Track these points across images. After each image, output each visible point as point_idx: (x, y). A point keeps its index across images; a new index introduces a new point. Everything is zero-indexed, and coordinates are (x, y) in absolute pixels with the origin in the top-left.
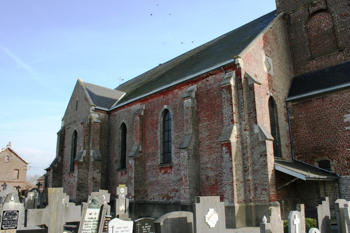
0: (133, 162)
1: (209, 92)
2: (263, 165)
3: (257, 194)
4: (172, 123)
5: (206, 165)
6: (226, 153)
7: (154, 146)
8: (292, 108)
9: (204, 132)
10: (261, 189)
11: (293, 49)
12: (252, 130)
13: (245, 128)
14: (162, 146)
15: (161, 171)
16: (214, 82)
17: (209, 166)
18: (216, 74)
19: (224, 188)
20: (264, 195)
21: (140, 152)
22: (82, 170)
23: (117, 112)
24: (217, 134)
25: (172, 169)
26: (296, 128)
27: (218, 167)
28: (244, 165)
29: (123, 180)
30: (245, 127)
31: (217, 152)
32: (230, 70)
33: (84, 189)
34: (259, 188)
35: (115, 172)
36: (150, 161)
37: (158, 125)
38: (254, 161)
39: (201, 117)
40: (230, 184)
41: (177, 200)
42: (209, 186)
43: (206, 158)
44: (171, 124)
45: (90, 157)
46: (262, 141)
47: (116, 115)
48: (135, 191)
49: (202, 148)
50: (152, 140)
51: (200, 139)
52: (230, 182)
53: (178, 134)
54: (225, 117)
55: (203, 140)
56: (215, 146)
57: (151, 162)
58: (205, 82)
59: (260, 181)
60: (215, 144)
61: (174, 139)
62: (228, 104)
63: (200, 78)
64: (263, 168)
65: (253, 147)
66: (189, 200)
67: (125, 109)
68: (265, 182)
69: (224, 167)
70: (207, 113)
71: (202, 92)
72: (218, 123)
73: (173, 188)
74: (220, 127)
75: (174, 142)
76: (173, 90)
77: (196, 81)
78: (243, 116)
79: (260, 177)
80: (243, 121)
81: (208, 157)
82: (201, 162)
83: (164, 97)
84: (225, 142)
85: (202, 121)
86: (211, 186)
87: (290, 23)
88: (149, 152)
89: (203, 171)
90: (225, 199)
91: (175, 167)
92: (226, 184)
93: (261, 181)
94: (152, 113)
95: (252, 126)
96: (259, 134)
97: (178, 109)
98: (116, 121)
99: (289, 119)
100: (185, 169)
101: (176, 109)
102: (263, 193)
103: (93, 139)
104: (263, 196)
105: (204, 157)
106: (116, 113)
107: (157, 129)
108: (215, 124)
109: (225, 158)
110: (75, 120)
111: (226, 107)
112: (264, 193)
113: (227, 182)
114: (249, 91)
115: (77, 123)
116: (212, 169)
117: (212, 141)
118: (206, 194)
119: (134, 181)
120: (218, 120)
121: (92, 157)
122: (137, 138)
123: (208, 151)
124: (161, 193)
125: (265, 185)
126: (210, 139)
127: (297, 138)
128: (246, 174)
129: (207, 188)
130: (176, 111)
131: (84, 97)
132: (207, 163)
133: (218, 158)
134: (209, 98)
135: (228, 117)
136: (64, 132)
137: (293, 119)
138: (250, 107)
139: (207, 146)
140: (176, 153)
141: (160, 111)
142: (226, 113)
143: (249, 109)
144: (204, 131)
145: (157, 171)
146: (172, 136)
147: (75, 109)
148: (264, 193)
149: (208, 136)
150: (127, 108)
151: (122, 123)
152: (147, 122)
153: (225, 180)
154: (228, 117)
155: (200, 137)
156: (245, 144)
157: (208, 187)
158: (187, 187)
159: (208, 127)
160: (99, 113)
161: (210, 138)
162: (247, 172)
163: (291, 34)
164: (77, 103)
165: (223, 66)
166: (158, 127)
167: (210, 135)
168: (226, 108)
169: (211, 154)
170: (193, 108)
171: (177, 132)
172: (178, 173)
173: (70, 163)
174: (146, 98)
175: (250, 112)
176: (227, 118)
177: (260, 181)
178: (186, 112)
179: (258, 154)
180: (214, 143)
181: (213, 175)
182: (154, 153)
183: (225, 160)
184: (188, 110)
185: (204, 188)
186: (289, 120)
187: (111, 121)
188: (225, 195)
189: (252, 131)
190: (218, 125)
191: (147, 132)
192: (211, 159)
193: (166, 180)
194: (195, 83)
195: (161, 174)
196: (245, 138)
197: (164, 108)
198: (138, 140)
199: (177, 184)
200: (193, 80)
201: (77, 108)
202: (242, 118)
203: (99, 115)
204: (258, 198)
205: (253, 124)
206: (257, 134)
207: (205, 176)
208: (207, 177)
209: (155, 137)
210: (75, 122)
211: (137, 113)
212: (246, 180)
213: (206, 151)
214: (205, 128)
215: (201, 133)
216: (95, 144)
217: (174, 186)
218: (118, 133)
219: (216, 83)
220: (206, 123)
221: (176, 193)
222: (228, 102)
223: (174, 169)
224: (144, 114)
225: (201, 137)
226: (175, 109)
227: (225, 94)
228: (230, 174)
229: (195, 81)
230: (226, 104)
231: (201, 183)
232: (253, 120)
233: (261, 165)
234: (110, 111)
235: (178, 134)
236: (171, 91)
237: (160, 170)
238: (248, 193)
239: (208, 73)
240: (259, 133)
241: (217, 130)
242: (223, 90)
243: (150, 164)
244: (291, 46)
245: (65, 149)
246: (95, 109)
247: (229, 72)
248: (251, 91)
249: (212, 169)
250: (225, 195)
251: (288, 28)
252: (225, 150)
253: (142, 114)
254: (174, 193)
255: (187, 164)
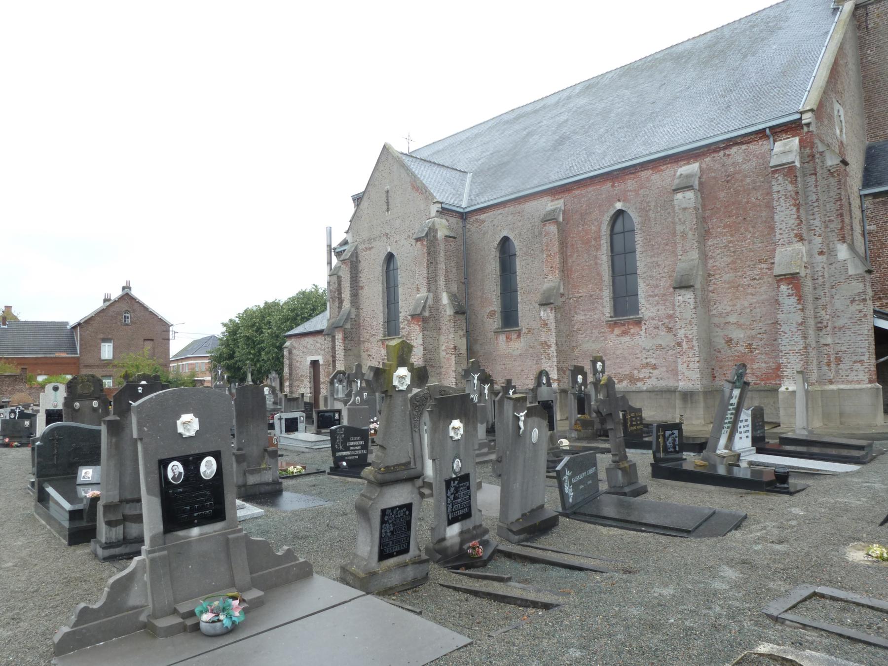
0: (550, 314)
1: (731, 179)
2: (856, 317)
3: (840, 371)
4: (639, 238)
5: (724, 317)
6: (788, 296)
7: (593, 283)
8: (872, 209)
9: (719, 256)
10: (851, 361)
11: (871, 83)
12: (832, 253)
13: (820, 250)
14: (611, 284)
15: (613, 330)
16: (744, 159)
17: (732, 319)
18: (751, 142)
19: (783, 359)
20: (857, 371)
21: (562, 295)
22: (428, 333)
23: (485, 215)
24: (752, 261)
25: (641, 327)
26: (878, 249)
27: (753, 321)
28: (816, 317)
29: (514, 350)
30: (820, 248)
31: (753, 295)
32: (784, 136)
33: (434, 370)
34: (846, 359)
35: (491, 335)
36: (582, 313)
37: (600, 241)
38: (835, 311)
39: (713, 228)
40: (797, 353)
41: (654, 384)
42: (732, 356)
43: (725, 305)
44: (636, 240)
45: (441, 307)
46: (855, 275)
47: (483, 221)
48: (558, 370)
49: (715, 286)
50: (588, 272)
51: (710, 270)
52: (799, 349)
53: (655, 259)
54: (780, 229)
55: (719, 272)
56: (746, 283)
57: (585, 314)
58: (721, 158)
59: (848, 347)
60: (748, 279)
61: (644, 270)
62: (788, 204)
63: (708, 150)
64: (857, 322)
65: (833, 284)
66: (699, 383)
67: (507, 209)
68: (859, 349)
69: (782, 322)
70: (727, 220)
71: (715, 178)
72: (755, 240)
73: (644, 361)
74: (759, 247)
75: (645, 275)
76: (639, 171)
77: (700, 155)
78: (816, 226)
79: (850, 340)
80: (816, 237)
81: (730, 303)
82: (714, 312)
83: (613, 186)
84: (787, 277)
85: (714, 235)
86: (738, 357)
87: (867, 27)
88: (580, 295)
89: (718, 330)
90: (785, 379)
91: (647, 323)
92: (789, 352)
93: (851, 347)
94: (585, 217)
95: (831, 246)
96: (849, 260)
97: (651, 212)
98: (484, 234)
99: (866, 231)
100: (689, 326)
101: (647, 211)
102: (855, 368)
103: (447, 271)
104: (855, 373)
105: (720, 303)
106: (483, 217)
107: (597, 249)
108: (747, 242)
109: (785, 305)
110: (388, 232)
111: (783, 209)
112: (857, 367)
113: (789, 348)
114: (826, 178)
115: (392, 238)
116: (741, 326)
117: (740, 274)
118: (726, 371)
119: (555, 351)
120: (754, 233)
121: (448, 306)
122: (551, 267)
123: (729, 293)
124: (614, 372)
125: (860, 354)
126: (736, 270)
127: (880, 267)
128: (821, 334)
129: (728, 360)
130: (647, 215)
131: (409, 184)
132: (728, 314)
133: (754, 305)
134: (732, 190)
135: (786, 228)
136: (357, 257)
137: (873, 230)
138: (828, 210)
139: (728, 283)
140: (650, 296)
141: (604, 214)
142: (783, 221)
143: (825, 213)
144: (718, 254)
145: (603, 330)
146: (638, 264)
147: (385, 207)
148: (857, 367)
149: (729, 264)
150: (512, 207)
151: (502, 237)
152: (572, 236)
153: (785, 346)
154: (786, 228)
155: (709, 265)
156: (820, 280)
157: (731, 358)
158: (692, 360)
159: (729, 247)
160: (448, 218)
161: (735, 267)
162: (823, 331)
163: (869, 52)
164: (387, 196)
165: (769, 128)
166: (600, 245)
167: (733, 262)
168: (782, 211)
169: (737, 298)
170: (696, 209)
171: (652, 257)
172: (656, 333)
173: (382, 320)
174: (567, 186)
175: (828, 219)
176: (785, 231)
177: (848, 347)
178: (681, 216)
179: (845, 297)
180: (745, 278)
181: (742, 336)
182: (594, 297)
183: (785, 308)
184: (686, 213)
185: (721, 361)
186: (866, 233)
187: (470, 233)
188: (786, 371)
189: (831, 256)
190: (753, 243)
191: (571, 256)
192: (738, 307)
193: (625, 347)
194: (696, 161)
195: (613, 337)
196: (820, 268)
197: (615, 208)
198: (555, 272)
199: (654, 355)
200: (691, 153)
201: (388, 206)
202: (813, 231)
203: (447, 221)
204: (844, 377)
205: (836, 242)
206: (845, 261)
207: (724, 338)
208: (729, 342)
209: (594, 266)
210: (387, 236)
211: (549, 219)
212: (821, 346)
213: (726, 293)
214: (721, 248)
215: (712, 257)
216: (450, 280)
217: (646, 358)
218: (492, 257)
219: (750, 160)
220: (725, 240)
221: (651, 371)
222: (788, 200)
223: (646, 327)
224: (563, 220)
225: (713, 267)
226: (644, 211)
227: (780, 184)
228: (797, 334)
229: (696, 156)
230: (783, 205)
231: (714, 352)
232: (834, 234)
233: (851, 318)
234: (466, 213)
235: (655, 259)
236: (633, 173)
237: (610, 328)
238: (825, 368)
239: (731, 141)
240: (848, 259)
241: (752, 254)
242: (776, 176)
243: (583, 317)
244: (864, 77)
245: (361, 291)
246: (442, 208)
247: (784, 139)
248: (831, 179)
249: (738, 325)
250: (786, 371)
251: (860, 38)
252: (786, 290)
253: (561, 219)
254: (649, 371)
255: (694, 316)
